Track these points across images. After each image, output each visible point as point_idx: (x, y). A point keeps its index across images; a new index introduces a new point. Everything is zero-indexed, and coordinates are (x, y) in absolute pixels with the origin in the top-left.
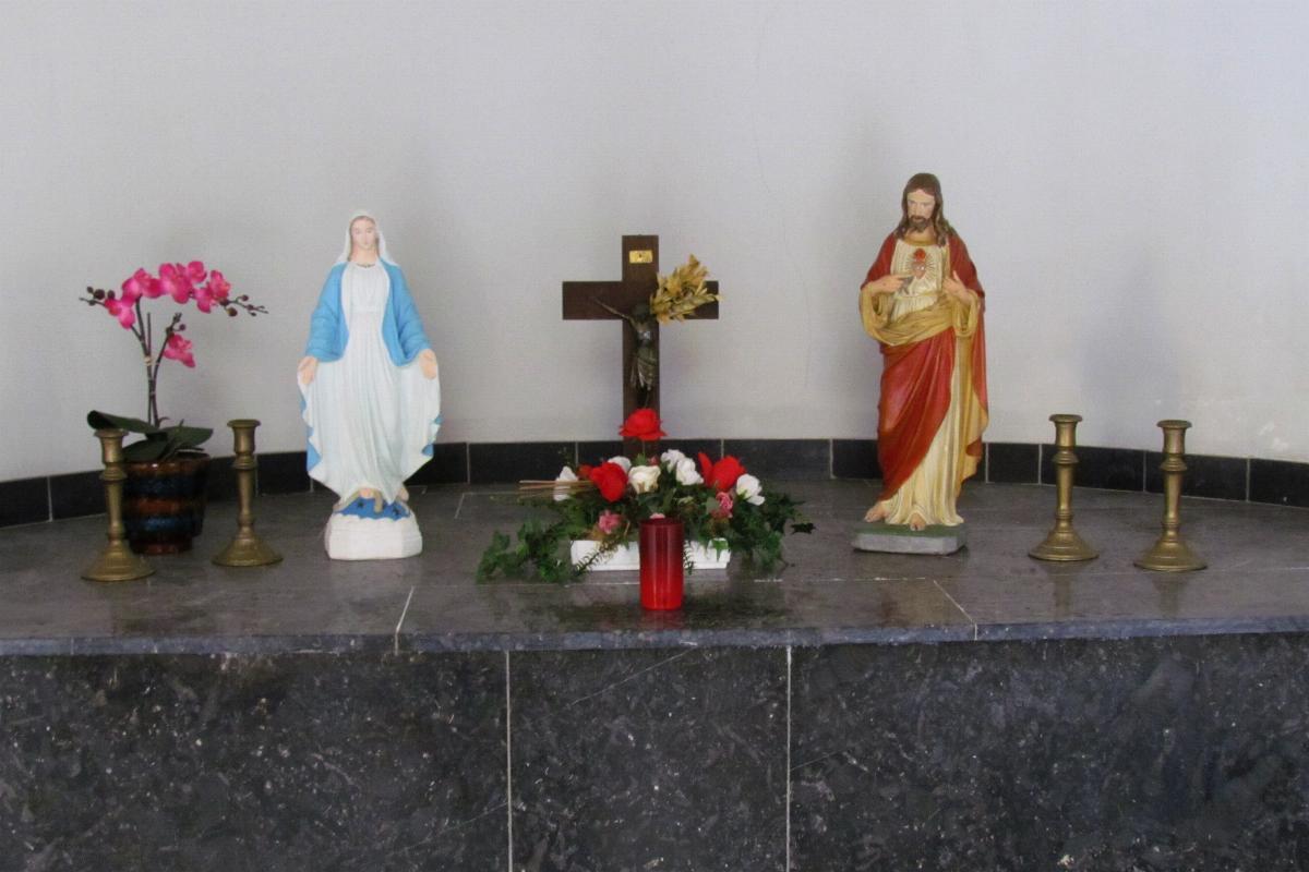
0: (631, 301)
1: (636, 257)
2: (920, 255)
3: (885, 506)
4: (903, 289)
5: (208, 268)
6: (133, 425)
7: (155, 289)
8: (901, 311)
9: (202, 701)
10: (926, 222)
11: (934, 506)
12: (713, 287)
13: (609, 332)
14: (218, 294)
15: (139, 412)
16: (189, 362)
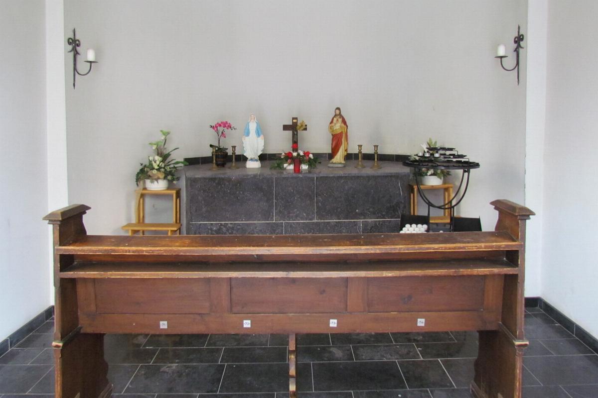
0: (294, 128)
1: (294, 121)
2: (337, 120)
3: (333, 160)
4: (335, 125)
5: (228, 122)
6: (216, 147)
7: (220, 125)
8: (335, 129)
9: (229, 184)
10: (338, 115)
11: (340, 160)
12: (306, 126)
13: (291, 132)
14: (230, 127)
15: (217, 145)
16: (225, 137)
